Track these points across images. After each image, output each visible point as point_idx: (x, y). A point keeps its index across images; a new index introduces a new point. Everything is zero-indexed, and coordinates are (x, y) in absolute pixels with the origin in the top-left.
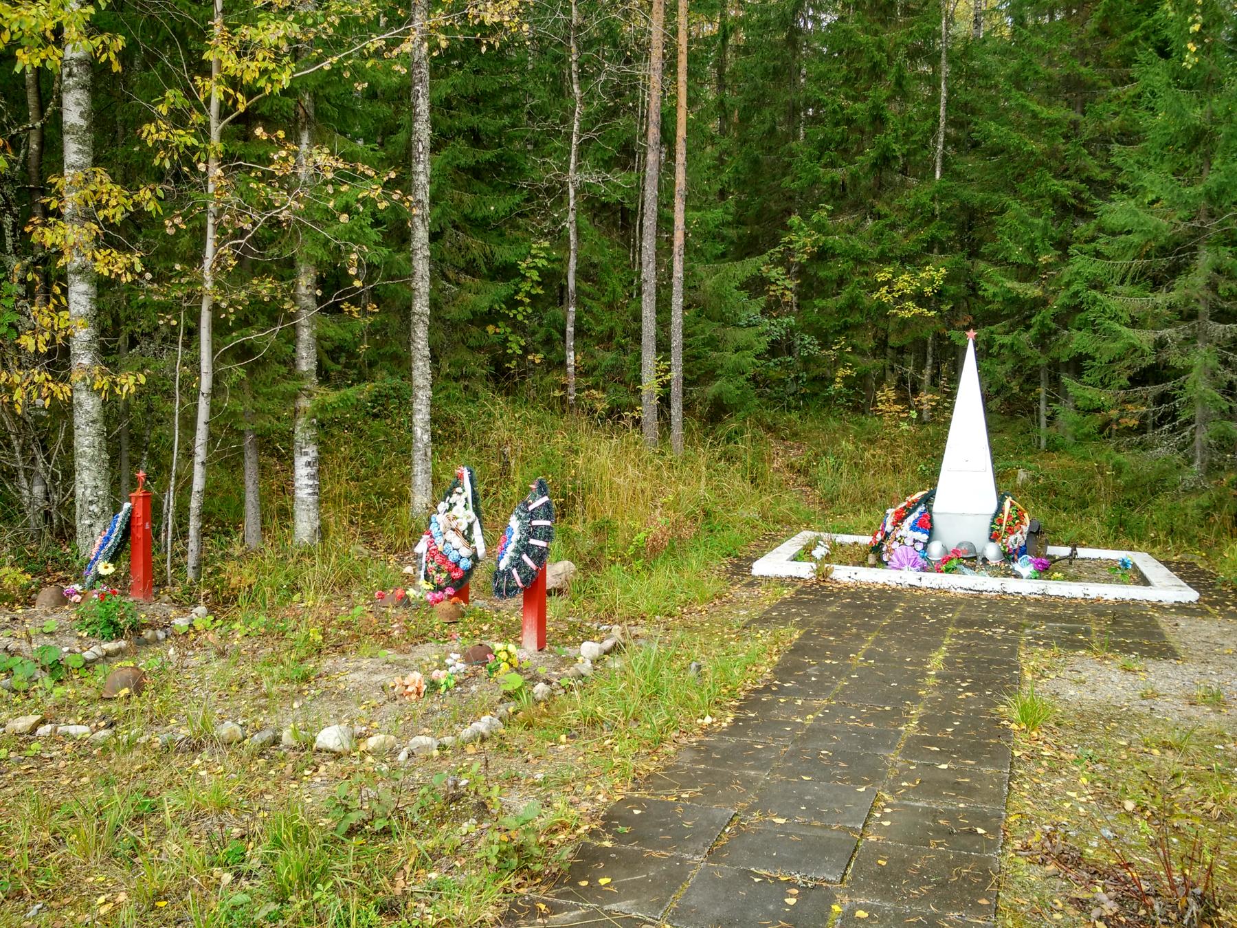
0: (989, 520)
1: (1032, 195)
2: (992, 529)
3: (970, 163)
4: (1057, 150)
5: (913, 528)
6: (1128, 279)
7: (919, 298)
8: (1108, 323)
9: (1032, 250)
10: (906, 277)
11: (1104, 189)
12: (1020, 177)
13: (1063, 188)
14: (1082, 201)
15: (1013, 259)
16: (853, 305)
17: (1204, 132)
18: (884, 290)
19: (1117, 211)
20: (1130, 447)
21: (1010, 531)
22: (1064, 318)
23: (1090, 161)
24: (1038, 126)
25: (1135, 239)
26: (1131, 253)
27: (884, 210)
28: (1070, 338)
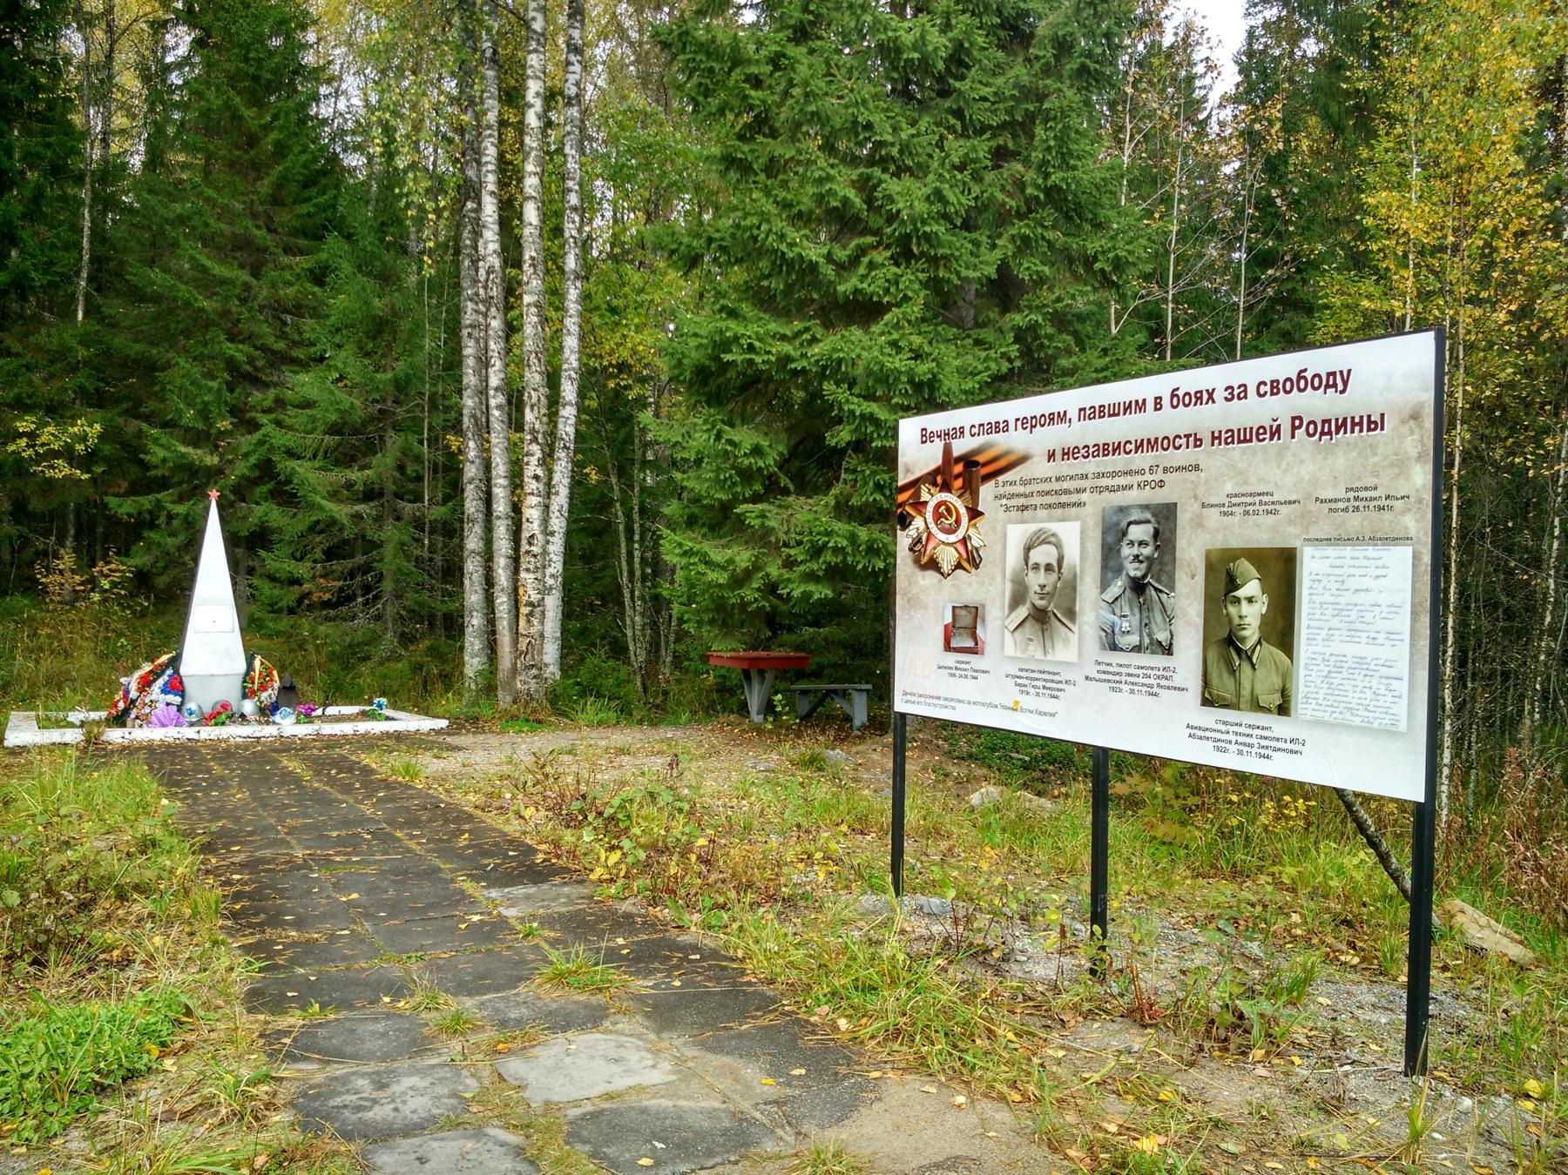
0: (240, 679)
1: (202, 354)
2: (244, 688)
3: (116, 308)
4: (229, 312)
5: (164, 691)
6: (321, 454)
9: (204, 414)
10: (51, 429)
11: (280, 360)
15: (184, 421)
17: (388, 322)
18: (23, 442)
19: (305, 383)
20: (328, 619)
21: (263, 688)
28: (250, 511)
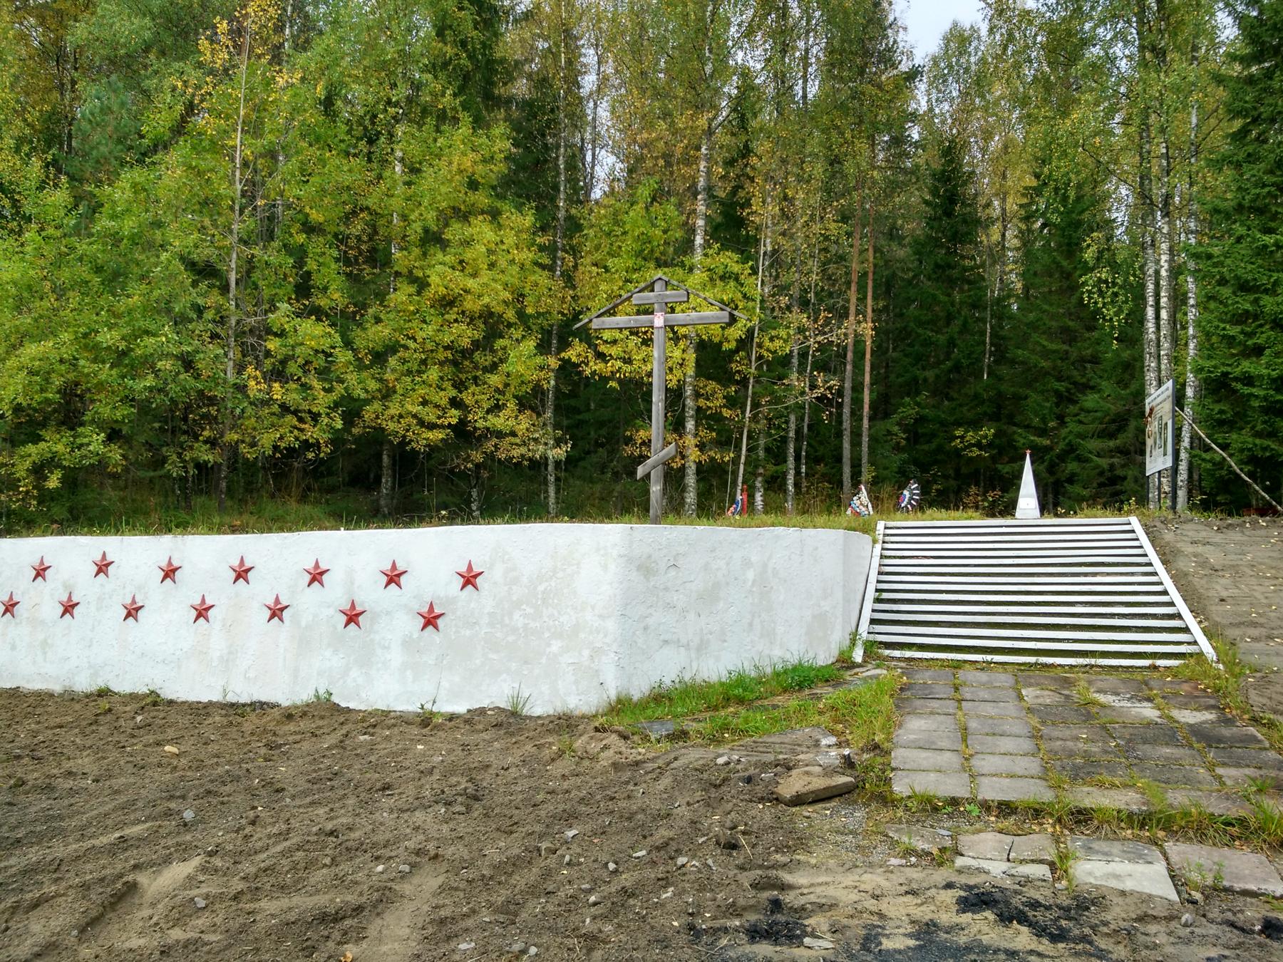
3: (1004, 370)
7: (979, 445)
8: (1086, 454)
9: (1044, 420)
10: (971, 433)
12: (1036, 380)
13: (1061, 386)
14: (1070, 394)
16: (940, 449)
18: (958, 441)
19: (1090, 400)
22: (1062, 457)
23: (1075, 373)
24: (1046, 354)
25: (1099, 414)
26: (1097, 422)
27: (955, 396)
